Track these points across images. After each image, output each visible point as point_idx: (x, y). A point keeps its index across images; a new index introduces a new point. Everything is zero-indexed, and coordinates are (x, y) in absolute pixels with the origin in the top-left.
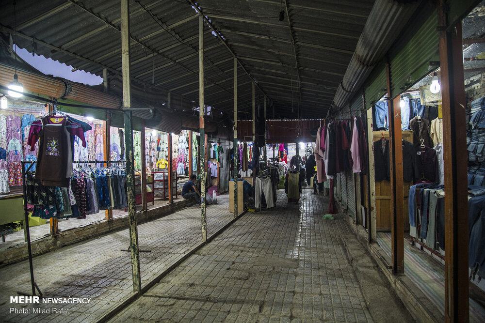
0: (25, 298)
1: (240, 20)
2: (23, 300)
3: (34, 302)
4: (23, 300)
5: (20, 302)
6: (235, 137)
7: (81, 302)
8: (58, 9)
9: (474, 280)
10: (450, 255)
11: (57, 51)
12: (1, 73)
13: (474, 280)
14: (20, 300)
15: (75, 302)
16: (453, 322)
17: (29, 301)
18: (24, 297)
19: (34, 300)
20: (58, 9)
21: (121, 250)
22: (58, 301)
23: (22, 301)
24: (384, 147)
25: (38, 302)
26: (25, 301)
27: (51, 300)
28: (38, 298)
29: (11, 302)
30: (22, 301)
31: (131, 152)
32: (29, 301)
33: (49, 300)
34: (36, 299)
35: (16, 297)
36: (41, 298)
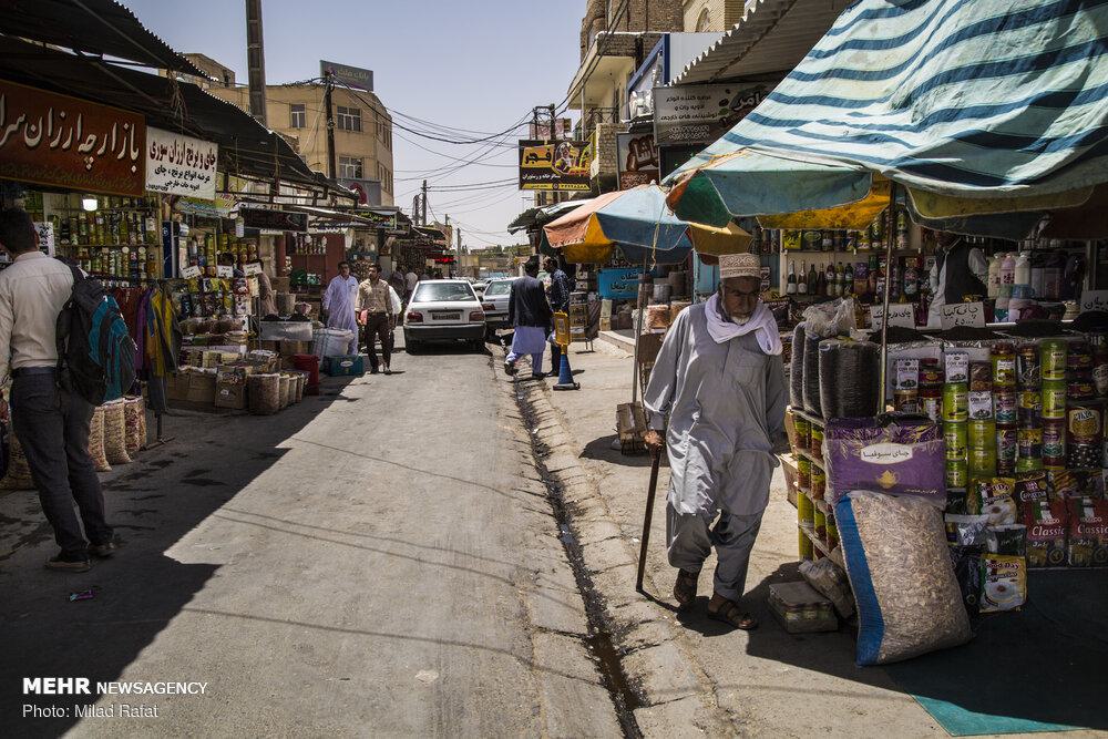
0: (175, 685)
4: (53, 685)
5: (47, 691)
7: (184, 692)
14: (47, 685)
18: (54, 680)
22: (133, 688)
23: (50, 689)
25: (99, 684)
28: (87, 681)
29: (26, 692)
30: (50, 689)
34: (82, 683)
35: (37, 680)
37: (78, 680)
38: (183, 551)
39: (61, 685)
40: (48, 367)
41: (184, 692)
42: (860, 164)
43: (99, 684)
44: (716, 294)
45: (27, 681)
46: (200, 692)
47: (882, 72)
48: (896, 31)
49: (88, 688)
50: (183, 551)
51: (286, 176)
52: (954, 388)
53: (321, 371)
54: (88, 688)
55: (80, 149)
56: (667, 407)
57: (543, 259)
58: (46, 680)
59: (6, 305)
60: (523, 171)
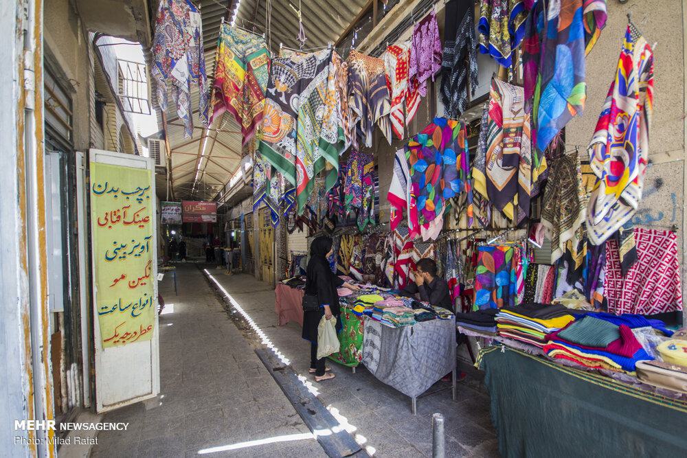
0: (108, 425)
2: (33, 425)
3: (48, 429)
4: (33, 425)
5: (29, 428)
6: (169, 309)
7: (114, 429)
8: (42, 373)
11: (628, 79)
14: (29, 425)
15: (106, 428)
16: (163, 3)
19: (49, 426)
20: (42, 373)
22: (82, 427)
23: (31, 427)
25: (61, 424)
26: (108, 428)
27: (72, 425)
30: (31, 427)
31: (93, 384)
33: (70, 425)
34: (51, 423)
35: (23, 422)
39: (38, 425)
41: (114, 429)
43: (61, 424)
44: (584, 13)
46: (124, 428)
47: (152, 84)
49: (55, 426)
51: (111, 96)
52: (402, 154)
54: (55, 426)
55: (325, 306)
59: (303, 167)
60: (57, 313)
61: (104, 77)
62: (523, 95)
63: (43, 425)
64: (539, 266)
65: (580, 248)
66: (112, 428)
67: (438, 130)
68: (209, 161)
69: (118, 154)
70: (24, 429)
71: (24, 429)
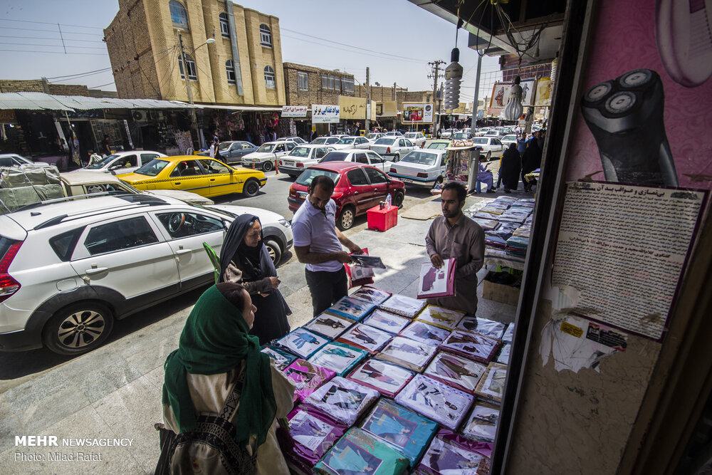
1: (567, 8)
4: (34, 440)
5: (30, 444)
7: (119, 445)
9: (371, 341)
10: (173, 324)
12: (181, 11)
13: (371, 341)
14: (30, 440)
17: (42, 443)
18: (34, 437)
19: (50, 441)
21: (368, 69)
22: (85, 443)
23: (32, 443)
24: (368, 285)
28: (56, 438)
29: (17, 444)
30: (32, 443)
32: (42, 443)
34: (53, 439)
36: (60, 439)
37: (50, 437)
38: (403, 267)
39: (39, 440)
40: (613, 162)
41: (119, 445)
42: (205, 208)
45: (17, 438)
48: (205, 52)
50: (403, 267)
53: (333, 198)
56: (700, 190)
57: (446, 181)
58: (30, 437)
61: (247, 186)
62: (594, 139)
63: (45, 440)
64: (661, 345)
65: (347, 243)
66: (116, 444)
67: (508, 231)
68: (289, 71)
69: (329, 122)
70: (25, 444)
71: (25, 444)
